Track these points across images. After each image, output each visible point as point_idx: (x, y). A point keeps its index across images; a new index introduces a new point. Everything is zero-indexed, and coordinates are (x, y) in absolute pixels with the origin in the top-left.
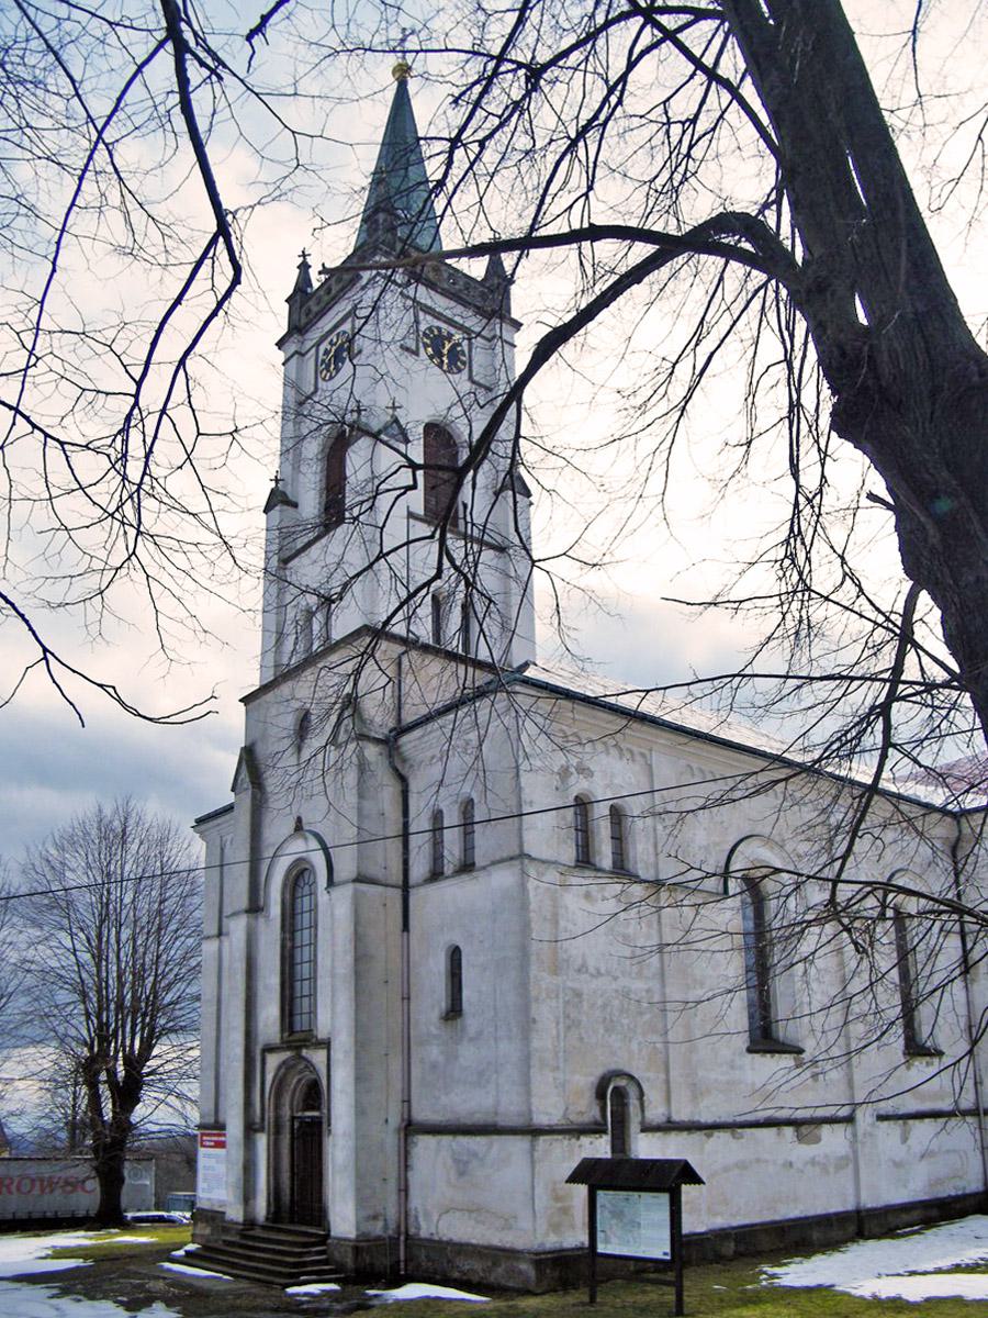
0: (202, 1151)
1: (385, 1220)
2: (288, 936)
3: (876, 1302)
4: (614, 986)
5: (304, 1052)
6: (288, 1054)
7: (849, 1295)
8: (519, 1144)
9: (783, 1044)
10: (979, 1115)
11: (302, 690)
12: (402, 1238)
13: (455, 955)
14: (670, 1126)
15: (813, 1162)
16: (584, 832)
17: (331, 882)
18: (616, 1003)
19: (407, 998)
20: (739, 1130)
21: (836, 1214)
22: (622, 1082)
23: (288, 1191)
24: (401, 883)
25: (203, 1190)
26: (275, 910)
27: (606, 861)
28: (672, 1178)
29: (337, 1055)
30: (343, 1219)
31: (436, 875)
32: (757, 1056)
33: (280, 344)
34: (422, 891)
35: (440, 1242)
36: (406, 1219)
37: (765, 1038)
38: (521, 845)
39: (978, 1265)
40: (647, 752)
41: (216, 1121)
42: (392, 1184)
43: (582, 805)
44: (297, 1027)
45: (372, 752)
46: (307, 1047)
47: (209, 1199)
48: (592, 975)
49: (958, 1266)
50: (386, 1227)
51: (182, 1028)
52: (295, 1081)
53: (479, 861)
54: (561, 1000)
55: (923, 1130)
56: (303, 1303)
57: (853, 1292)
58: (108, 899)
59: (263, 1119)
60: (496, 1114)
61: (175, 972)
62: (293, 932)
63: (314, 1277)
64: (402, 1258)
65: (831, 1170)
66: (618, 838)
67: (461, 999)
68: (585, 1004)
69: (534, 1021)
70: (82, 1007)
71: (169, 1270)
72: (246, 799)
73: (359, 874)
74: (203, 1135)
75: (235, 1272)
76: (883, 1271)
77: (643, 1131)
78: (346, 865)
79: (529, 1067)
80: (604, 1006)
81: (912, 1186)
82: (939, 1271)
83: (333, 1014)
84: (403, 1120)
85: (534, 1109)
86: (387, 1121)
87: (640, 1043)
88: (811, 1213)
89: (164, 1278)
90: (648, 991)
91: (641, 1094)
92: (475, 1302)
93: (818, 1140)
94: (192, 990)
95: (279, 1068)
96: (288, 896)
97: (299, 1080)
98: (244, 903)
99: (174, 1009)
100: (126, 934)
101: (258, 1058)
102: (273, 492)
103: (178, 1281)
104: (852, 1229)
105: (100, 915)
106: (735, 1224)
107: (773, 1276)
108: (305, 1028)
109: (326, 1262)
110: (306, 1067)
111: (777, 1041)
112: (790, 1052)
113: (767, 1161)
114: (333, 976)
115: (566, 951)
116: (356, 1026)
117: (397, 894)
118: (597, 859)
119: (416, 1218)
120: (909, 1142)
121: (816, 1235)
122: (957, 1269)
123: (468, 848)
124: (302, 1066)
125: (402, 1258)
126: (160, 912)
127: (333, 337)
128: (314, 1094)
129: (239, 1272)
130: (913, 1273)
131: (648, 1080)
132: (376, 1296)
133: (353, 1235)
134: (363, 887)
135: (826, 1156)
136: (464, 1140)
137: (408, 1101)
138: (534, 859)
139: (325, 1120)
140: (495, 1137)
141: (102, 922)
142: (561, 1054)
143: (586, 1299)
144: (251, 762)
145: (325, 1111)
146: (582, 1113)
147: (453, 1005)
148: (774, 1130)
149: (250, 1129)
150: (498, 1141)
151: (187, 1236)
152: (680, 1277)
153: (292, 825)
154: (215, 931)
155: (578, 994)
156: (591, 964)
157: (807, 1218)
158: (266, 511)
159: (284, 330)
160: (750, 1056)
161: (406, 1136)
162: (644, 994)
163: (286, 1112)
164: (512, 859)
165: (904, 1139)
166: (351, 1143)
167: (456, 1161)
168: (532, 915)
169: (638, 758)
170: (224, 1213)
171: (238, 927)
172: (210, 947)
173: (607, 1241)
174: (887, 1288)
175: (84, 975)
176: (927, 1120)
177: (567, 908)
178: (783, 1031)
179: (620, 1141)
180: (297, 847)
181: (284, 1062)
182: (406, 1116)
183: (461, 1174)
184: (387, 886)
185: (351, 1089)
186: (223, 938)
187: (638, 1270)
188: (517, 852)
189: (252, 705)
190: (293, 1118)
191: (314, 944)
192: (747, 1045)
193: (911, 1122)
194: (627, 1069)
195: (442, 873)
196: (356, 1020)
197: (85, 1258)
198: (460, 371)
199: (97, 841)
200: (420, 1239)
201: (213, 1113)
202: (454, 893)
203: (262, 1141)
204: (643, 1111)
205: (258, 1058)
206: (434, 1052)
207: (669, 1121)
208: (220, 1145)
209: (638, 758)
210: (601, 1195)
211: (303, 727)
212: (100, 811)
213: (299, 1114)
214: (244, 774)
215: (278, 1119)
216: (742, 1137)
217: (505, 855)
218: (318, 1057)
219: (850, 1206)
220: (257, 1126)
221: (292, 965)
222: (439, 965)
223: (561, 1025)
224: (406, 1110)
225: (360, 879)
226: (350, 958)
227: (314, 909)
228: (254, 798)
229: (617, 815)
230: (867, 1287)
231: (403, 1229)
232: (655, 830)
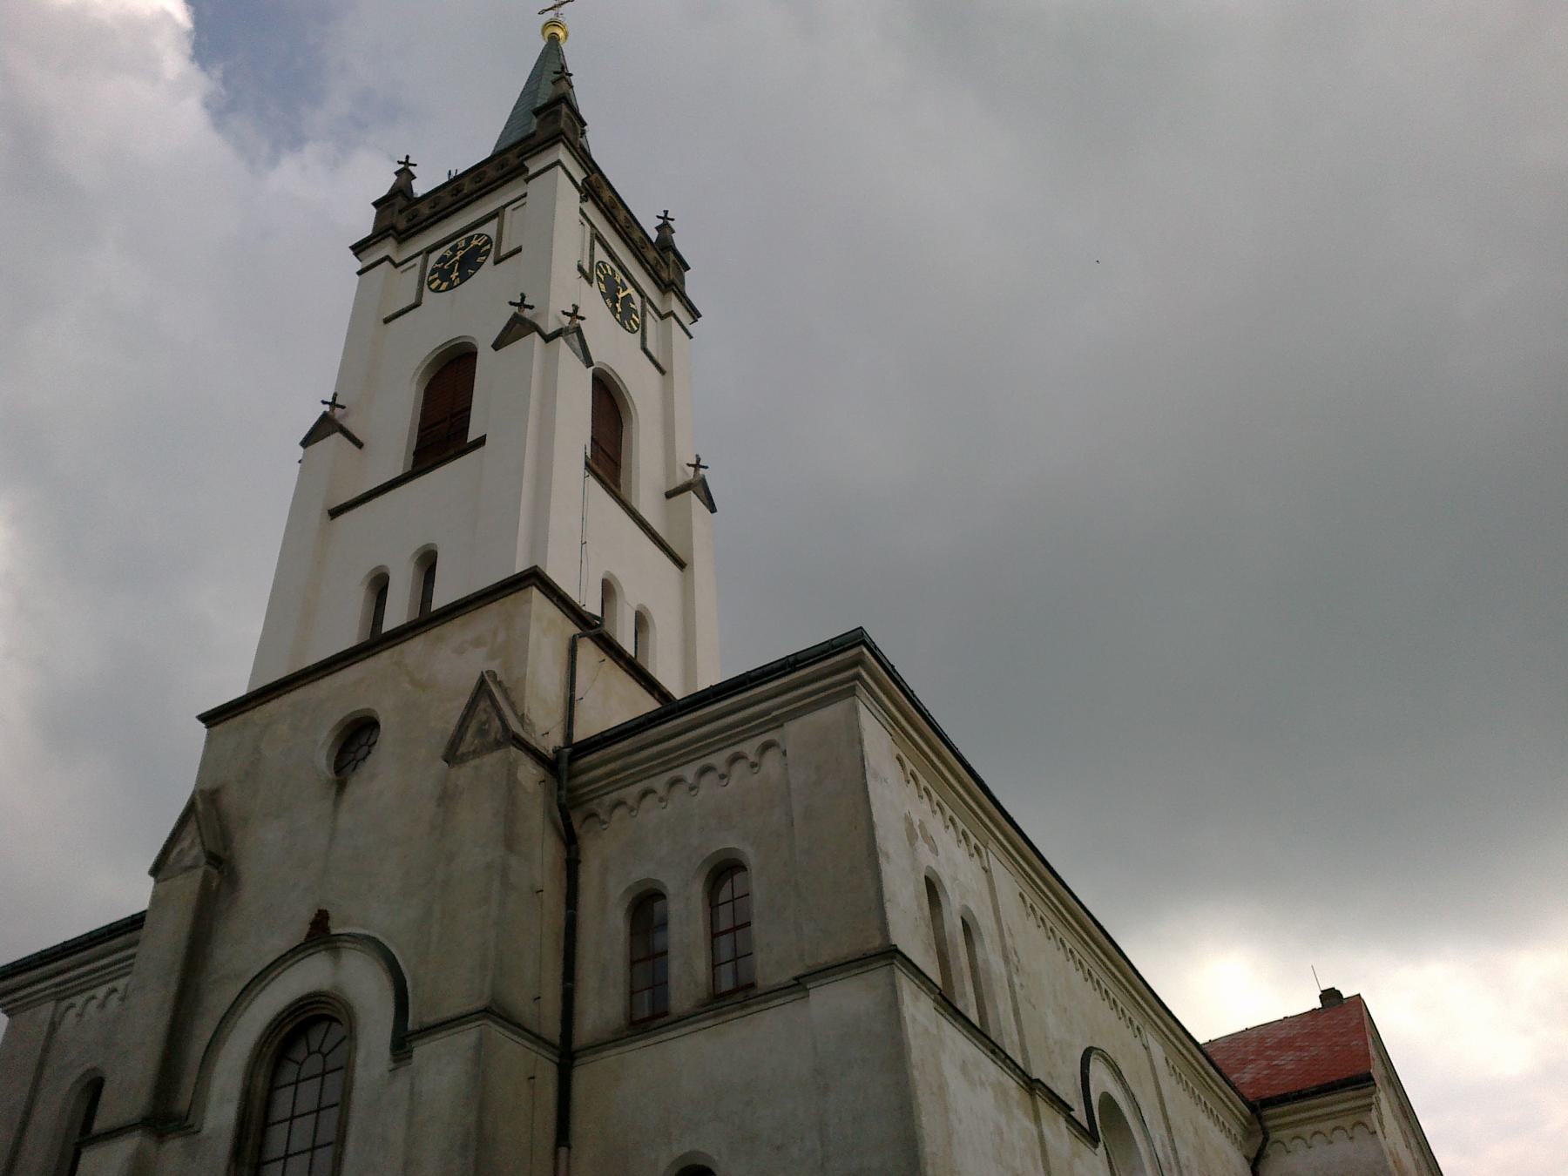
31: (648, 1017)
33: (359, 249)
34: (611, 1057)
53: (769, 967)
99: (469, 240)
127: (461, 242)
158: (306, 443)
159: (366, 230)
202: (693, 1060)
211: (357, 735)
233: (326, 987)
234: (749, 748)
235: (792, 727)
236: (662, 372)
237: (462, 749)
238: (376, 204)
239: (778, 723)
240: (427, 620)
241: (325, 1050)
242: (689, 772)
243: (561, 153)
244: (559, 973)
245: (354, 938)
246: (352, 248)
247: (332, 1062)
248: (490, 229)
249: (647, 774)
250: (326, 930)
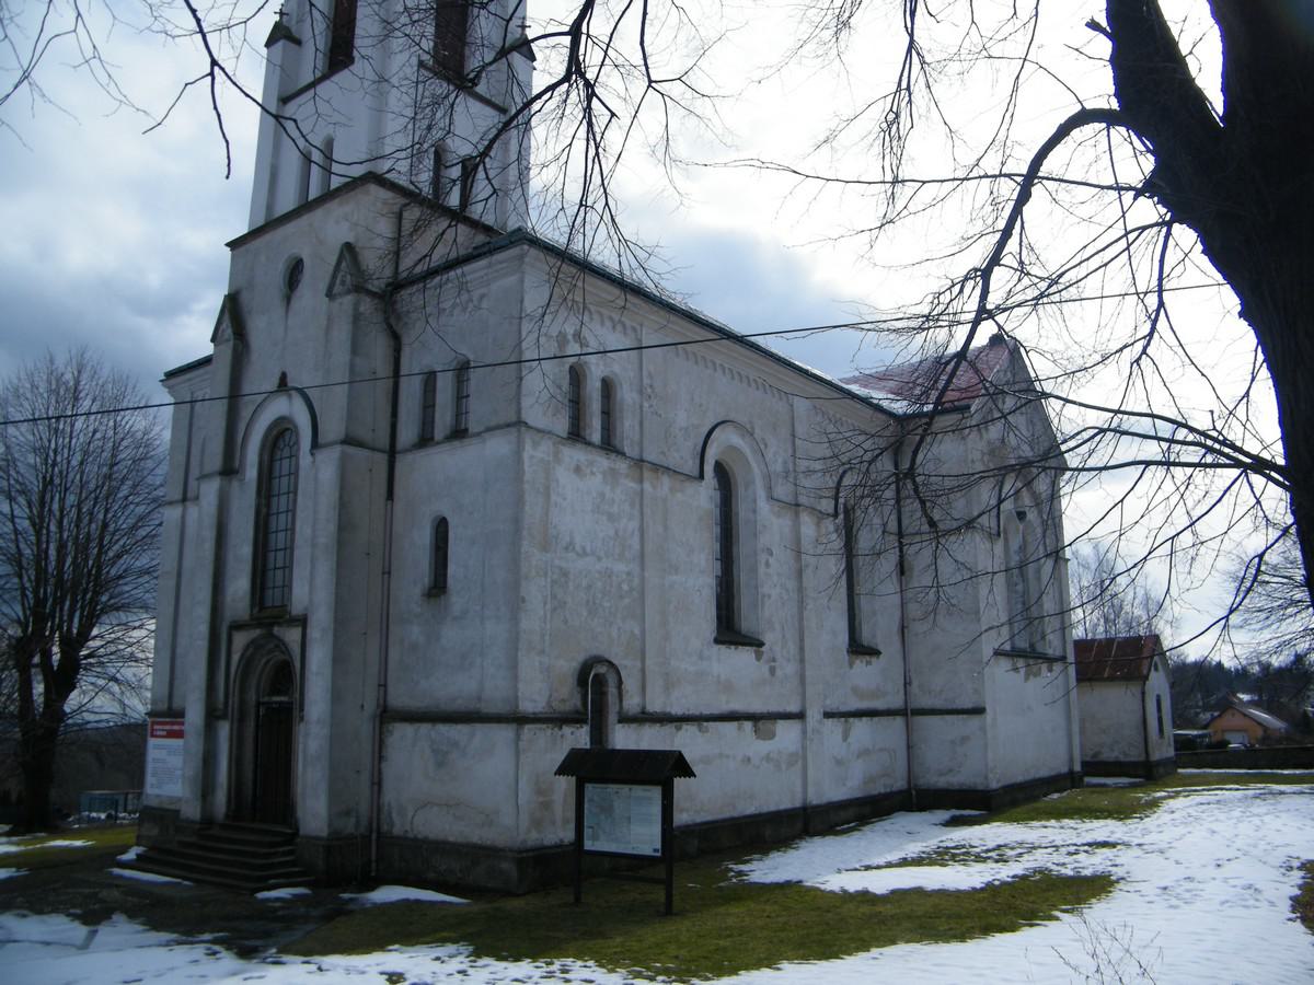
0: (152, 742)
1: (357, 817)
2: (263, 501)
3: (846, 896)
4: (598, 567)
5: (276, 630)
6: (256, 633)
7: (818, 889)
8: (504, 733)
9: (745, 636)
10: (907, 715)
11: (293, 240)
12: (374, 836)
13: (441, 528)
14: (645, 718)
15: (768, 758)
16: (576, 404)
17: (315, 445)
18: (599, 584)
19: (387, 573)
20: (705, 724)
21: (786, 811)
22: (602, 669)
23: (250, 784)
24: (388, 447)
25: (152, 785)
26: (251, 473)
27: (596, 437)
28: (666, 769)
29: (314, 633)
30: (314, 810)
31: (425, 440)
32: (723, 647)
34: (409, 457)
35: (415, 840)
36: (378, 815)
37: (729, 630)
38: (519, 411)
39: (923, 859)
40: (638, 327)
41: (170, 708)
42: (365, 777)
43: (577, 376)
44: (269, 603)
45: (367, 305)
46: (279, 624)
47: (158, 796)
48: (578, 554)
49: (905, 859)
50: (358, 823)
51: (123, 606)
52: (264, 660)
53: (473, 427)
54: (549, 580)
55: (861, 727)
56: (276, 910)
57: (823, 887)
58: (55, 460)
59: (226, 703)
60: (479, 699)
61: (121, 543)
62: (269, 497)
63: (282, 881)
64: (374, 858)
65: (784, 767)
66: (607, 413)
67: (445, 575)
68: (571, 584)
69: (523, 600)
70: (16, 580)
71: (121, 877)
72: (227, 350)
73: (347, 436)
74: (153, 723)
75: (194, 876)
76: (842, 866)
77: (620, 722)
78: (333, 428)
79: (517, 649)
80: (589, 587)
81: (849, 784)
82: (889, 865)
83: (311, 586)
84: (378, 706)
85: (520, 694)
86: (362, 706)
87: (619, 629)
88: (765, 809)
89: (117, 886)
90: (628, 574)
91: (620, 682)
92: (457, 904)
93: (771, 735)
94: (144, 561)
95: (247, 648)
96: (266, 458)
97: (268, 661)
98: (215, 461)
100: (71, 499)
101: (224, 636)
102: (277, 26)
103: (133, 888)
104: (799, 826)
105: (44, 478)
106: (698, 820)
107: (741, 873)
108: (278, 603)
109: (293, 863)
110: (277, 646)
111: (738, 633)
112: (750, 645)
113: (728, 757)
114: (314, 545)
115: (555, 527)
116: (336, 603)
117: (382, 459)
118: (588, 432)
119: (390, 813)
120: (849, 740)
121: (768, 832)
122: (904, 863)
123: (460, 412)
124: (271, 646)
125: (374, 858)
126: (109, 477)
128: (286, 675)
129: (199, 877)
130: (868, 868)
131: (626, 667)
132: (351, 900)
133: (324, 833)
134: (351, 450)
135: (780, 752)
136: (443, 728)
137: (383, 686)
138: (531, 428)
139: (296, 706)
140: (478, 726)
141: (45, 487)
142: (547, 638)
143: (571, 899)
144: (234, 313)
145: (297, 696)
146: (563, 701)
147: (435, 581)
148: (736, 723)
149: (212, 716)
150: (481, 730)
151: (130, 836)
152: (670, 873)
153: (275, 381)
154: (178, 496)
155: (565, 574)
156: (578, 541)
157: (760, 815)
158: (268, 45)
160: (716, 647)
161: (381, 723)
162: (624, 576)
163: (252, 697)
164: (508, 425)
165: (845, 737)
166: (326, 731)
167: (435, 752)
168: (526, 486)
169: (629, 331)
170: (178, 812)
171: (210, 490)
172: (172, 514)
173: (595, 838)
174: (853, 882)
175: (22, 546)
176: (864, 719)
177: (557, 481)
178: (746, 624)
179: (599, 733)
180: (279, 407)
181: (253, 642)
182: (382, 702)
183: (440, 764)
184: (373, 449)
185: (328, 671)
186: (188, 504)
187: (628, 866)
188: (514, 419)
189: (238, 251)
190: (258, 704)
191: (292, 511)
192: (714, 635)
193: (851, 720)
194: (607, 656)
195: (432, 438)
196: (337, 595)
197: (19, 867)
199: (45, 395)
200: (392, 837)
201: (166, 699)
202: (444, 462)
203: (224, 730)
204: (621, 701)
205: (224, 636)
206: (416, 632)
207: (643, 713)
208: (179, 735)
209: (629, 331)
210: (590, 788)
211: (295, 271)
212: (52, 361)
213: (266, 699)
214: (227, 323)
215: (242, 702)
216: (707, 731)
217: (501, 422)
218: (292, 636)
219: (798, 804)
220: (218, 713)
221: (266, 533)
222: (424, 537)
223: (548, 606)
224: (382, 692)
225: (349, 441)
226: (332, 527)
227: (294, 473)
228: (235, 350)
229: (608, 387)
230: (835, 882)
231: (375, 825)
232: (641, 407)
240: (328, 196)
244: (389, 414)
245: (297, 389)
250: (286, 385)
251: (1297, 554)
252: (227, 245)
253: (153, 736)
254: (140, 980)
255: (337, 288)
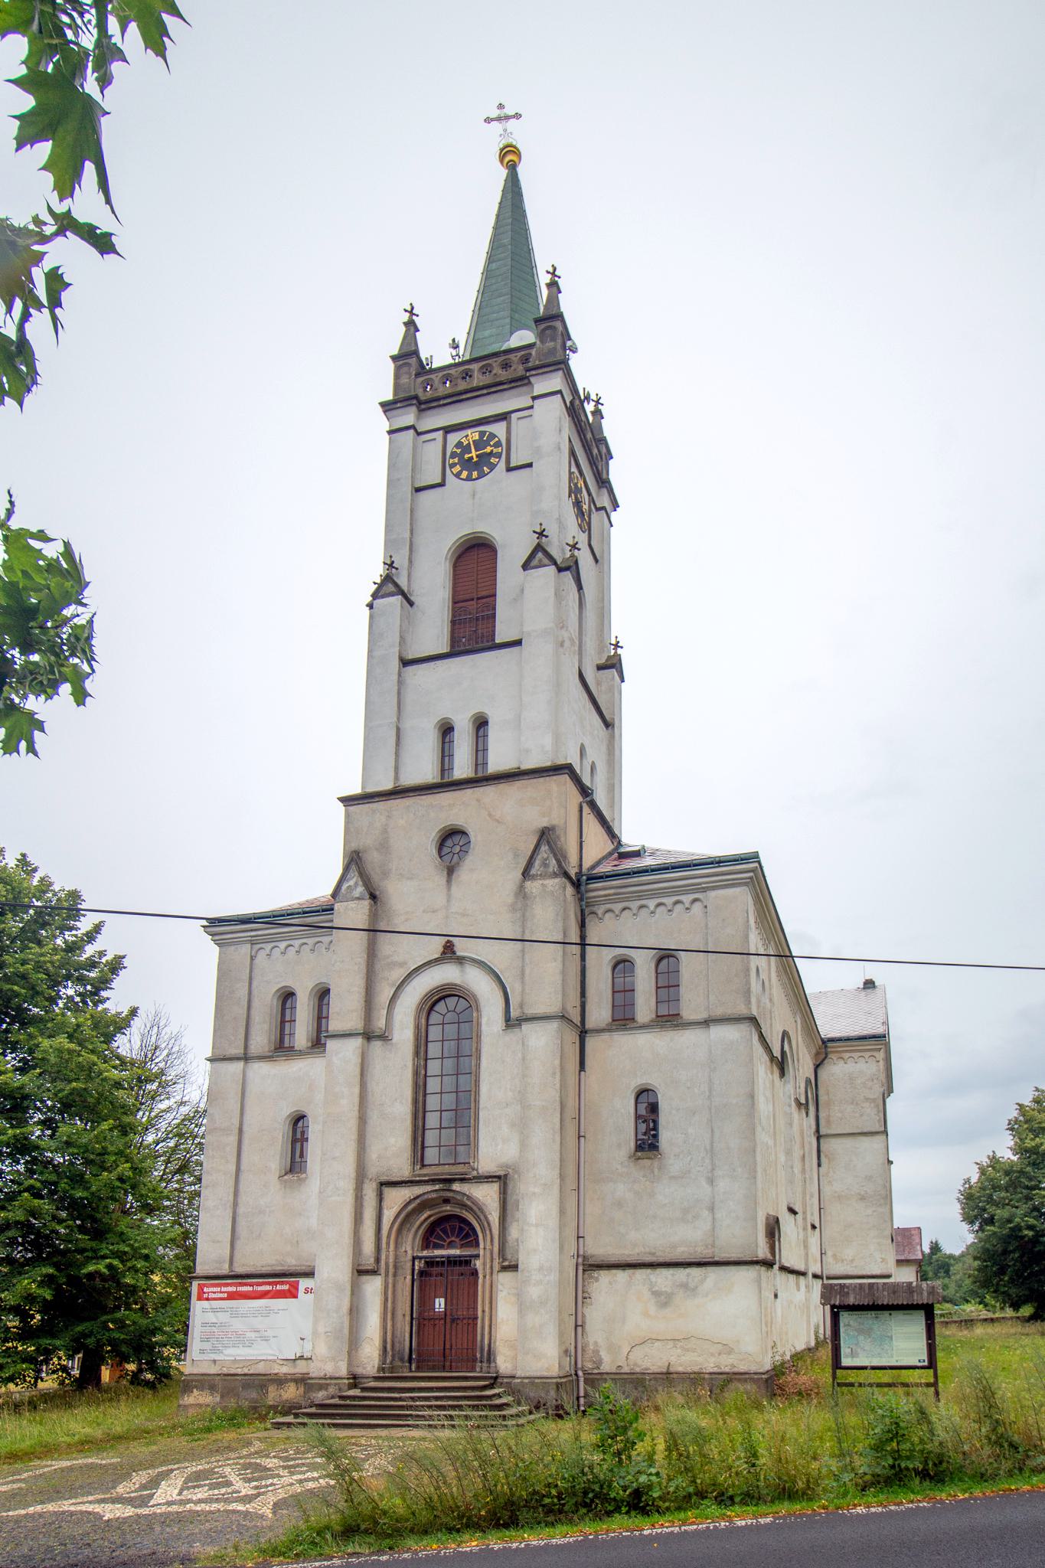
31: (623, 1019)
53: (688, 1013)
198: (492, 467)
233: (458, 982)
234: (687, 899)
235: (713, 894)
236: (597, 561)
237: (533, 872)
238: (394, 358)
239: (705, 890)
241: (458, 1010)
242: (652, 904)
243: (555, 382)
246: (383, 405)
247: (463, 1017)
248: (499, 429)
249: (627, 900)
251: (1042, 1485)
252: (343, 800)
253: (200, 1298)
254: (889, 1276)
255: (536, 868)
